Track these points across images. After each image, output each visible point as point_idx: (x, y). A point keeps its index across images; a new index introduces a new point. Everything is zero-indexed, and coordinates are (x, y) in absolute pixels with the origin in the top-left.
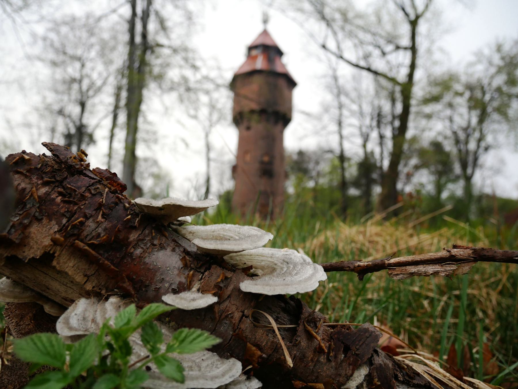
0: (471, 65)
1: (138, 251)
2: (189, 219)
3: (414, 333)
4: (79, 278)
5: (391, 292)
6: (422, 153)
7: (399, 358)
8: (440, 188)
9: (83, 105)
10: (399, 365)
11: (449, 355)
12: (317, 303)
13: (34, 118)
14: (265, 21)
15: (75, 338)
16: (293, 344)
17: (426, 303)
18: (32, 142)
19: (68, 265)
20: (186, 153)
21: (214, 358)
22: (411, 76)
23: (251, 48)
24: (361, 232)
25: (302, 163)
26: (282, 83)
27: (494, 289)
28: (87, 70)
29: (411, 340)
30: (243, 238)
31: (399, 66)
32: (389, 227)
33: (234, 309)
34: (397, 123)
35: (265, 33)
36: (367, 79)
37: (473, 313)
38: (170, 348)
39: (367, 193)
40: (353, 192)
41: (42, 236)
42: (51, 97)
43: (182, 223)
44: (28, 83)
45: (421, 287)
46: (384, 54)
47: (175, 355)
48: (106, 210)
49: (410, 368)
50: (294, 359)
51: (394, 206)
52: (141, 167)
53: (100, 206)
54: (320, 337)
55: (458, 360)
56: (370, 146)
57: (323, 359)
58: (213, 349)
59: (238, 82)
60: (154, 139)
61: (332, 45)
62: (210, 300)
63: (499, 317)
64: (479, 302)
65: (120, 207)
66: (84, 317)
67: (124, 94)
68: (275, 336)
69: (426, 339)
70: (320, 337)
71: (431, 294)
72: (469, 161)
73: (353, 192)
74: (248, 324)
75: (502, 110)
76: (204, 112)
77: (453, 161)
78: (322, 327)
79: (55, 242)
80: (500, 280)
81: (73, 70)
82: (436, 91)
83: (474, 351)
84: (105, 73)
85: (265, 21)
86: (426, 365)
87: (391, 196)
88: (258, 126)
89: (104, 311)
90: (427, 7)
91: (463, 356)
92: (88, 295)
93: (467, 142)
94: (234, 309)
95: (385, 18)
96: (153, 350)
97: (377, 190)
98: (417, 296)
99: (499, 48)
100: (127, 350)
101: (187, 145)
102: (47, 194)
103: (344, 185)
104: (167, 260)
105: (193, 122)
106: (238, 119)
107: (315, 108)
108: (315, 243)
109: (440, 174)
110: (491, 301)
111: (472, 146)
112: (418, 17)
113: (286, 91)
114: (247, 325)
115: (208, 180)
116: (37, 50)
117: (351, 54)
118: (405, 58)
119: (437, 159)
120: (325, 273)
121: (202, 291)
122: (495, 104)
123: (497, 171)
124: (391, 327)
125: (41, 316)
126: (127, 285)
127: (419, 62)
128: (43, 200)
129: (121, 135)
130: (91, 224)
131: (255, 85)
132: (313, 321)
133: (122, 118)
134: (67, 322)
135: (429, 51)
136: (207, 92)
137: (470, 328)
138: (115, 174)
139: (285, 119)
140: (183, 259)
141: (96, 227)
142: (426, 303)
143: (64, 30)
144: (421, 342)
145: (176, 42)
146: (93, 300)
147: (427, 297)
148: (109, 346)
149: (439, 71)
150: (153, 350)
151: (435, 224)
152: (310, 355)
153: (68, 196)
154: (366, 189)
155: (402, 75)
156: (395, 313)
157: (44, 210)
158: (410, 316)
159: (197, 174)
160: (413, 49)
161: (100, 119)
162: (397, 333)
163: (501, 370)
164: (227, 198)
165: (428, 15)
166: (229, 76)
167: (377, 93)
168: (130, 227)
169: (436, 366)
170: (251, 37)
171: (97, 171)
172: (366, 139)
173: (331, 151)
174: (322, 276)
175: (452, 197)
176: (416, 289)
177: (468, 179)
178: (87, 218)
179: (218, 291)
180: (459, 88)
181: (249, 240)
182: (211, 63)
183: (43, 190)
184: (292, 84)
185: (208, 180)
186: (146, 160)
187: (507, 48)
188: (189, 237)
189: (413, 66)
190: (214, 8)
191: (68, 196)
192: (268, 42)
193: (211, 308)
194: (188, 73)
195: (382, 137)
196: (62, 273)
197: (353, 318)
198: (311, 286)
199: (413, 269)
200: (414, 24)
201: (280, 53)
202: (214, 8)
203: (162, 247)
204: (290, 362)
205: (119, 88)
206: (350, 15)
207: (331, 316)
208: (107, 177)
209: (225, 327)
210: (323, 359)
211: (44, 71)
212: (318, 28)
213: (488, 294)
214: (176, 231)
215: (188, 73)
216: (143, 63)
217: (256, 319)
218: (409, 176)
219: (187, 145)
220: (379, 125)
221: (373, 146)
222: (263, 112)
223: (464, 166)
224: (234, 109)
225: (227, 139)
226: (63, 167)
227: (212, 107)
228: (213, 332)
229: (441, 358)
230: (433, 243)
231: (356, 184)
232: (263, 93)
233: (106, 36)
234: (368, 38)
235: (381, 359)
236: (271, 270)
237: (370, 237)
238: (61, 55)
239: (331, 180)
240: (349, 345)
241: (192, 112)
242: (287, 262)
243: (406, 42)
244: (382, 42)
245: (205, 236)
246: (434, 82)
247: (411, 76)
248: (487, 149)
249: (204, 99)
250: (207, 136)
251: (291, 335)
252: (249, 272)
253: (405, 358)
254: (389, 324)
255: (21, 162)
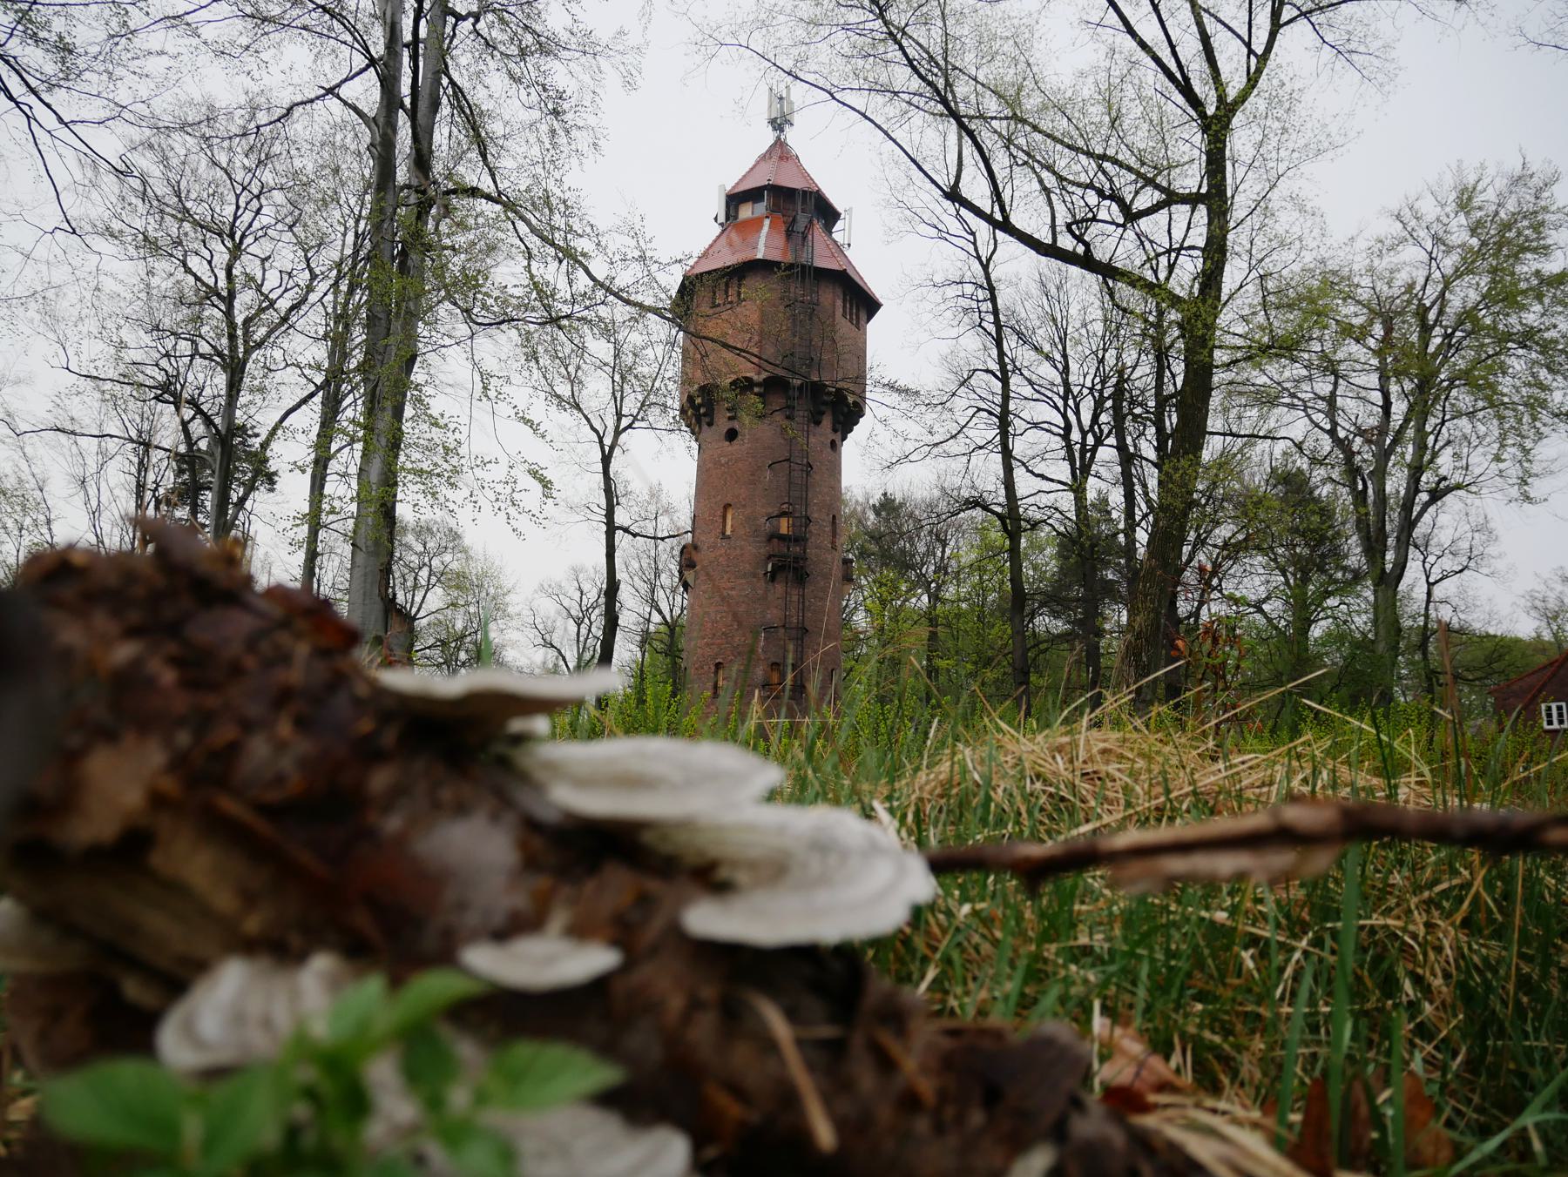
0: (1387, 246)
1: (393, 823)
2: (541, 724)
3: (1213, 1048)
4: (224, 901)
5: (1142, 925)
6: (1249, 506)
7: (1149, 1121)
8: (1303, 614)
9: (235, 371)
10: (1144, 1143)
11: (1307, 1114)
12: (925, 960)
13: (87, 409)
14: (779, 124)
15: (214, 1074)
16: (836, 1085)
17: (1247, 957)
18: (89, 506)
19: (196, 864)
20: (540, 514)
21: (607, 1126)
22: (1211, 279)
23: (735, 200)
24: (1060, 749)
25: (893, 537)
26: (831, 298)
27: (1448, 915)
28: (248, 264)
29: (1200, 1068)
30: (696, 779)
31: (1175, 251)
32: (1139, 736)
33: (667, 985)
34: (1172, 420)
35: (780, 151)
36: (1083, 288)
37: (1390, 986)
38: (481, 1098)
39: (1089, 627)
40: (1047, 623)
41: (121, 782)
42: (140, 345)
43: (521, 739)
44: (67, 305)
45: (1233, 911)
46: (1131, 216)
47: (495, 1117)
48: (304, 707)
49: (1174, 1148)
50: (840, 1125)
51: (1172, 667)
52: (410, 549)
53: (283, 697)
54: (914, 1061)
55: (1334, 1125)
56: (1093, 487)
57: (922, 1125)
58: (607, 1100)
59: (698, 296)
60: (447, 469)
61: (976, 189)
62: (589, 961)
63: (1467, 995)
64: (1405, 949)
65: (341, 702)
66: (238, 1013)
67: (358, 335)
68: (782, 1062)
69: (1248, 1067)
70: (914, 1061)
71: (1265, 932)
72: (1389, 533)
73: (1047, 623)
74: (706, 1023)
75: (1481, 381)
76: (597, 390)
77: (1354, 525)
78: (925, 1033)
79: (157, 800)
80: (1466, 886)
81: (209, 262)
82: (1284, 322)
83: (1380, 1099)
84: (296, 263)
85: (779, 124)
86: (1224, 1139)
87: (1160, 633)
88: (761, 431)
89: (295, 995)
90: (1252, 80)
91: (1349, 1111)
92: (248, 947)
93: (1380, 474)
94: (667, 985)
95: (1132, 112)
96: (434, 1103)
97: (1118, 616)
98: (1221, 936)
99: (1465, 202)
100: (357, 1103)
101: (546, 484)
102: (136, 664)
103: (1019, 602)
104: (474, 848)
105: (569, 418)
106: (699, 411)
107: (930, 376)
108: (924, 781)
109: (1304, 569)
110: (1439, 949)
111: (1396, 483)
112: (1228, 109)
113: (844, 326)
114: (703, 1031)
115: (612, 590)
116: (98, 203)
117: (1031, 216)
118: (1191, 225)
119: (1293, 520)
120: (932, 881)
121: (579, 932)
122: (1460, 362)
123: (1471, 561)
124: (1142, 1033)
125: (111, 1010)
126: (362, 920)
127: (1237, 239)
128: (127, 682)
129: (347, 458)
130: (258, 749)
131: (753, 305)
132: (895, 1017)
133: (352, 410)
134: (189, 1031)
135: (1260, 204)
136: (608, 331)
137: (1374, 1028)
138: (326, 604)
139: (844, 411)
140: (523, 846)
141: (273, 755)
142: (1247, 957)
143: (181, 144)
144: (1234, 1074)
145: (514, 180)
146: (264, 962)
147: (1254, 941)
148: (310, 1094)
149: (1289, 265)
150: (434, 1103)
151: (1283, 723)
152: (885, 1113)
153: (198, 668)
154: (1093, 611)
155: (1185, 275)
156: (1160, 987)
157: (125, 706)
158: (1201, 997)
159: (576, 572)
160: (1215, 199)
161: (282, 403)
162: (1163, 1048)
163: (1458, 1152)
164: (666, 644)
165: (1255, 102)
166: (672, 280)
167: (1112, 332)
168: (369, 753)
169: (1254, 1143)
170: (738, 157)
171: (278, 593)
172: (1082, 468)
173: (976, 503)
174: (920, 885)
175: (1338, 637)
176: (1221, 916)
177: (1388, 582)
178: (247, 726)
179: (621, 933)
180: (1353, 314)
181: (711, 784)
182: (618, 243)
183: (124, 652)
184: (864, 304)
185: (612, 590)
186: (423, 531)
187: (1487, 198)
188: (540, 775)
189: (1216, 251)
190: (629, 84)
191: (198, 668)
192: (789, 181)
193: (599, 986)
194: (552, 272)
195: (1128, 459)
196: (175, 889)
197: (1025, 1004)
198: (888, 917)
199: (1176, 865)
200: (1216, 128)
201: (828, 214)
202: (629, 84)
203: (461, 810)
204: (825, 1134)
205: (343, 318)
206: (1031, 103)
207: (965, 1003)
208: (303, 609)
209: (643, 1041)
210: (922, 1125)
211: (121, 269)
212: (935, 139)
213: (1429, 926)
214: (504, 763)
215: (552, 272)
216: (418, 243)
217: (733, 1016)
218: (1208, 580)
219: (546, 484)
220: (1119, 429)
221: (1104, 484)
222: (774, 385)
223: (1374, 545)
224: (686, 381)
225: (666, 469)
226: (175, 586)
227: (622, 374)
228: (607, 1050)
229: (1281, 1120)
230: (1271, 778)
231: (1055, 601)
232: (773, 331)
233: (307, 163)
234: (1082, 169)
235: (1092, 1124)
236: (776, 870)
237: (1096, 764)
238: (172, 221)
239: (982, 590)
240: (1001, 1084)
241: (564, 389)
242: (822, 846)
243: (1191, 180)
244: (1125, 182)
245: (587, 776)
246: (1274, 299)
247: (1211, 279)
248: (1436, 495)
249: (600, 348)
250: (606, 460)
251: (830, 1058)
252: (710, 877)
253: (1170, 1120)
254: (1138, 1022)
255: (55, 573)
